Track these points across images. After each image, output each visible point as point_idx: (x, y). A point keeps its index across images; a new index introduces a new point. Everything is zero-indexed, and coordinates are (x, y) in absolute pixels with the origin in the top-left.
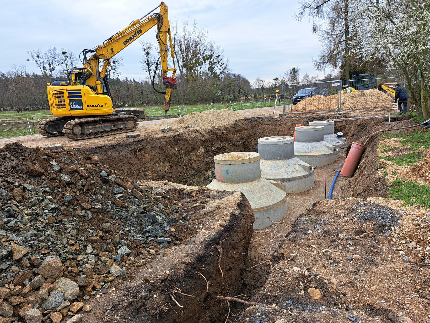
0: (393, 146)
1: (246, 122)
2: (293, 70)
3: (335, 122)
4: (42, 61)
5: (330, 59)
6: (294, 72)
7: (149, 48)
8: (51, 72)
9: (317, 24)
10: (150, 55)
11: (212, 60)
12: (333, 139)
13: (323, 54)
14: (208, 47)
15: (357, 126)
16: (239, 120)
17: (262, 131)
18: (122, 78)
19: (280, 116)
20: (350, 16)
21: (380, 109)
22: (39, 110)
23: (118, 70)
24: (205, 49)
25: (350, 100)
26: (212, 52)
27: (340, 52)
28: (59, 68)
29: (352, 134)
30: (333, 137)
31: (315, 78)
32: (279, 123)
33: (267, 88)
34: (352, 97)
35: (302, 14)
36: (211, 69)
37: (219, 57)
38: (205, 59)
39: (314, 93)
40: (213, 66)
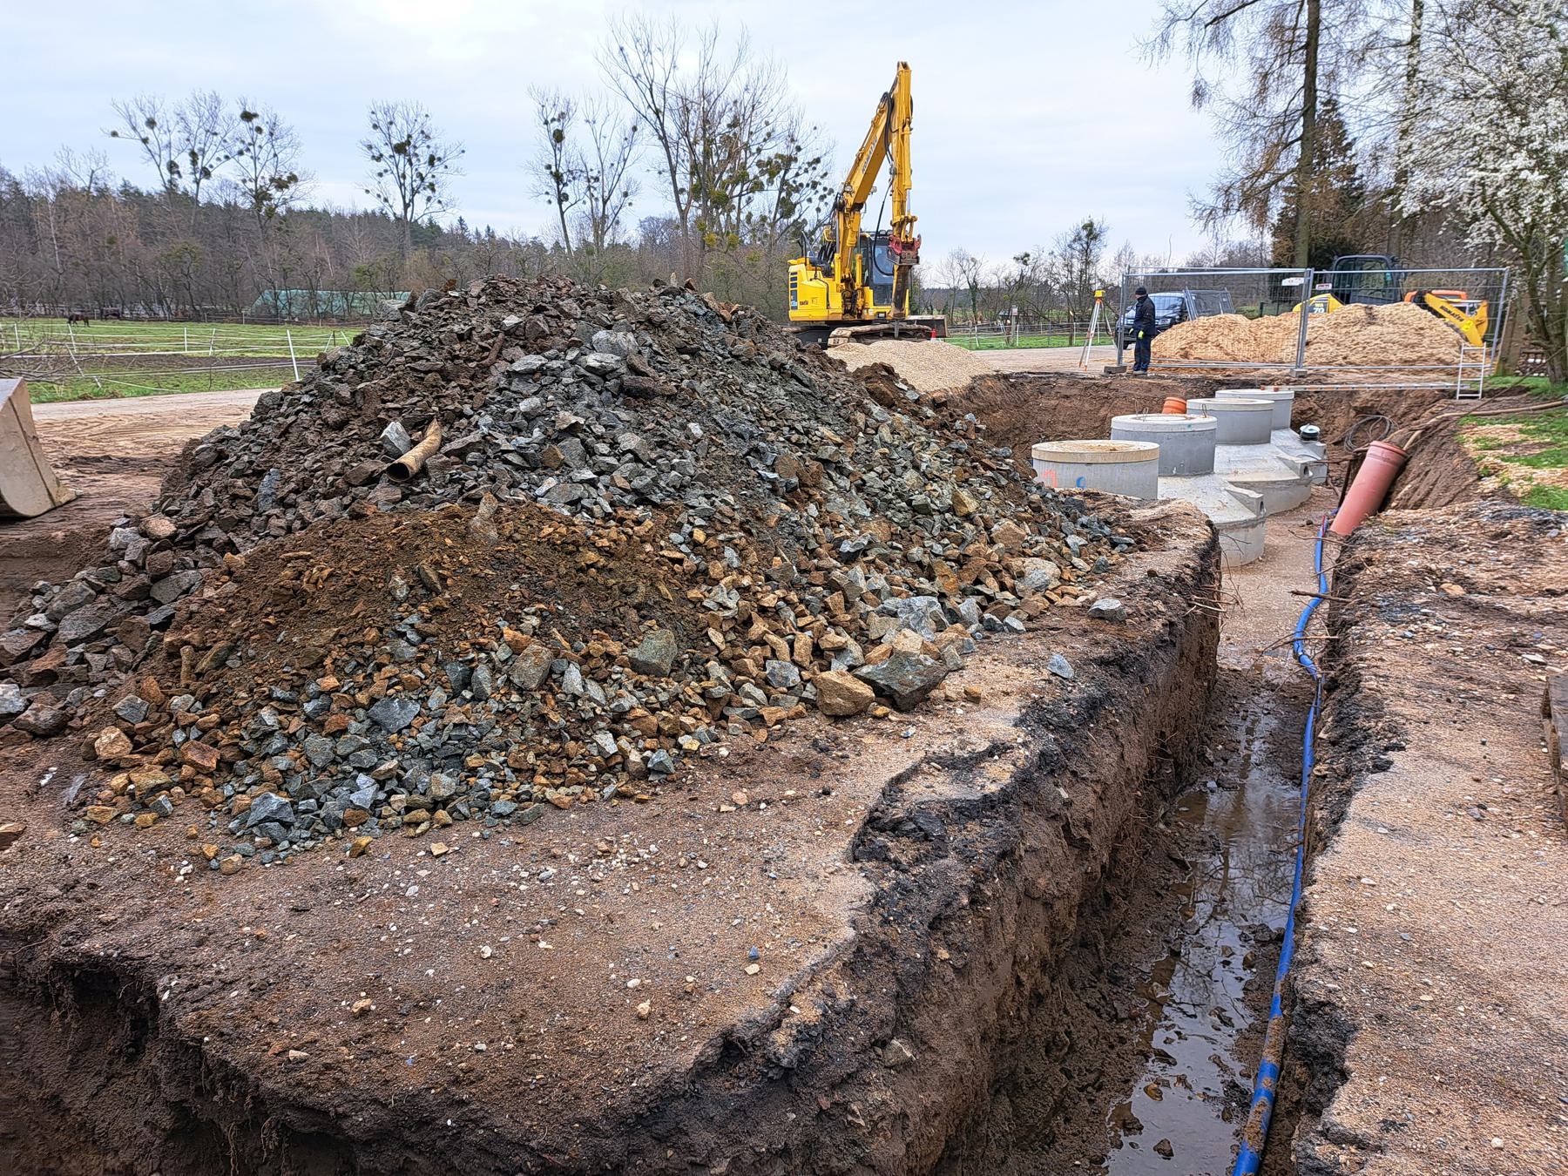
0: (1504, 438)
1: (1001, 385)
2: (1085, 227)
3: (1297, 395)
4: (165, 139)
5: (1246, 200)
6: (1091, 233)
7: (562, 115)
8: (197, 182)
9: (1210, 77)
10: (566, 142)
11: (790, 175)
12: (1290, 443)
13: (1226, 182)
14: (781, 128)
15: (1353, 414)
16: (982, 378)
17: (1047, 418)
18: (446, 222)
19: (1109, 371)
20: (1325, 55)
21: (1423, 366)
22: (155, 319)
23: (443, 193)
24: (769, 135)
25: (1330, 333)
26: (793, 146)
27: (1281, 178)
28: (226, 172)
29: (1337, 436)
30: (1285, 439)
31: (1157, 261)
32: (1105, 393)
33: (989, 289)
34: (1338, 325)
35: (1164, 41)
36: (786, 207)
37: (819, 166)
38: (772, 168)
39: (1191, 309)
40: (795, 197)
